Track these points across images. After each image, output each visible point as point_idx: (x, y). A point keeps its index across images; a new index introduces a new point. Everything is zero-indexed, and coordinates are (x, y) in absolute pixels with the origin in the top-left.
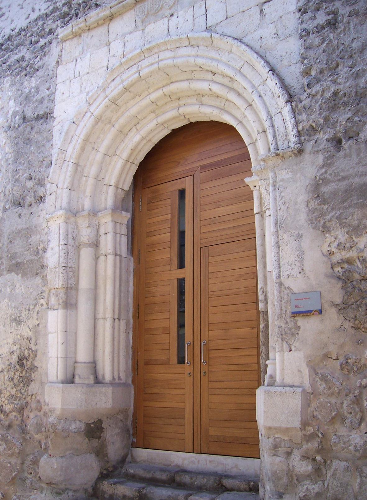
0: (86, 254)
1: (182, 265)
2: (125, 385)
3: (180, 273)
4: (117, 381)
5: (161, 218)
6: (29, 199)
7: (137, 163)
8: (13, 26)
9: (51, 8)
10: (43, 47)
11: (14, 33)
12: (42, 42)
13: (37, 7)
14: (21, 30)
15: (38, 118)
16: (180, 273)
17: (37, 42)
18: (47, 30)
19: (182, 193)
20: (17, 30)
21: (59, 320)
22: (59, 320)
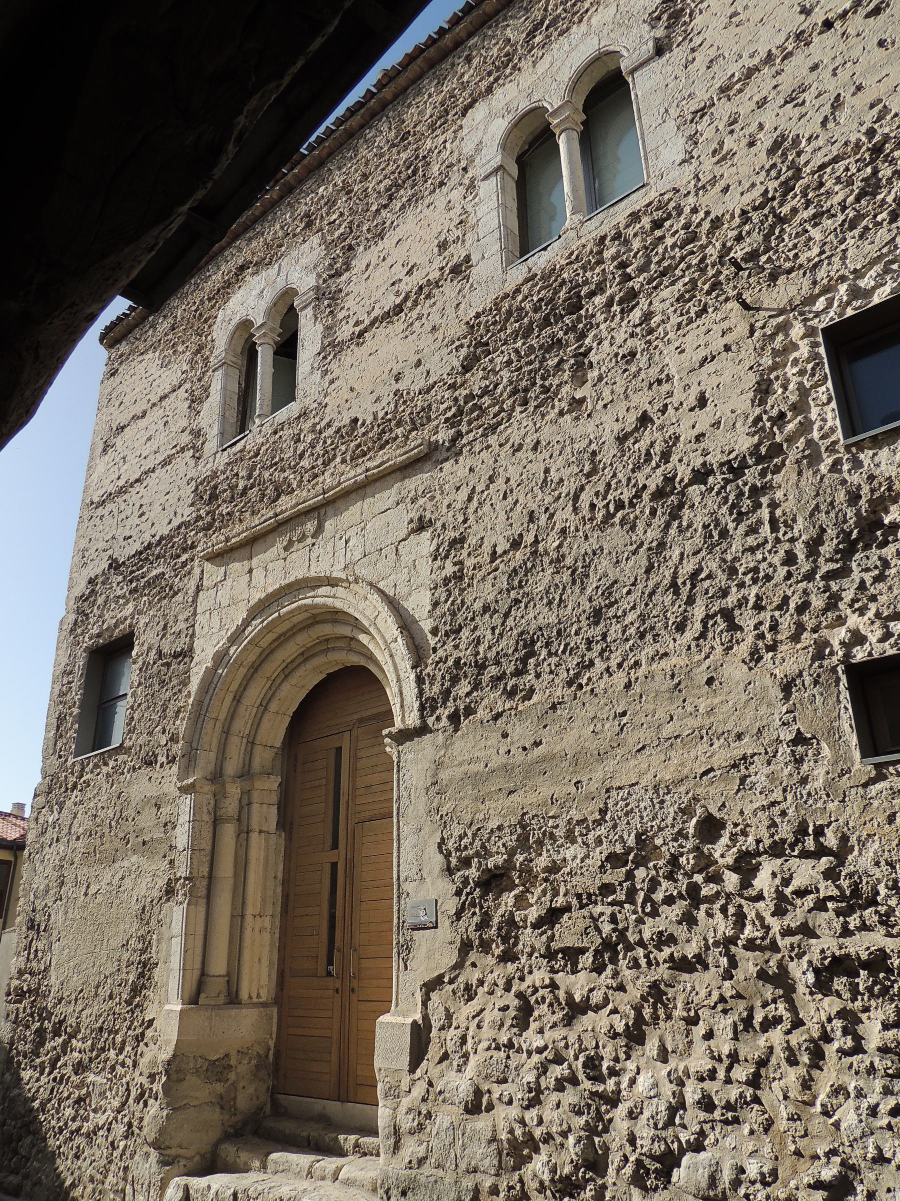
0: (229, 831)
1: (335, 846)
2: (264, 1005)
3: (332, 856)
4: (255, 1000)
5: (317, 783)
6: (162, 759)
7: (291, 713)
8: (153, 532)
9: (194, 515)
10: (184, 564)
11: (153, 541)
12: (184, 558)
13: (179, 511)
14: (162, 538)
15: (176, 656)
16: (332, 856)
17: (178, 556)
18: (189, 543)
19: (339, 750)
20: (157, 538)
21: (311, 502)
22: (311, 502)
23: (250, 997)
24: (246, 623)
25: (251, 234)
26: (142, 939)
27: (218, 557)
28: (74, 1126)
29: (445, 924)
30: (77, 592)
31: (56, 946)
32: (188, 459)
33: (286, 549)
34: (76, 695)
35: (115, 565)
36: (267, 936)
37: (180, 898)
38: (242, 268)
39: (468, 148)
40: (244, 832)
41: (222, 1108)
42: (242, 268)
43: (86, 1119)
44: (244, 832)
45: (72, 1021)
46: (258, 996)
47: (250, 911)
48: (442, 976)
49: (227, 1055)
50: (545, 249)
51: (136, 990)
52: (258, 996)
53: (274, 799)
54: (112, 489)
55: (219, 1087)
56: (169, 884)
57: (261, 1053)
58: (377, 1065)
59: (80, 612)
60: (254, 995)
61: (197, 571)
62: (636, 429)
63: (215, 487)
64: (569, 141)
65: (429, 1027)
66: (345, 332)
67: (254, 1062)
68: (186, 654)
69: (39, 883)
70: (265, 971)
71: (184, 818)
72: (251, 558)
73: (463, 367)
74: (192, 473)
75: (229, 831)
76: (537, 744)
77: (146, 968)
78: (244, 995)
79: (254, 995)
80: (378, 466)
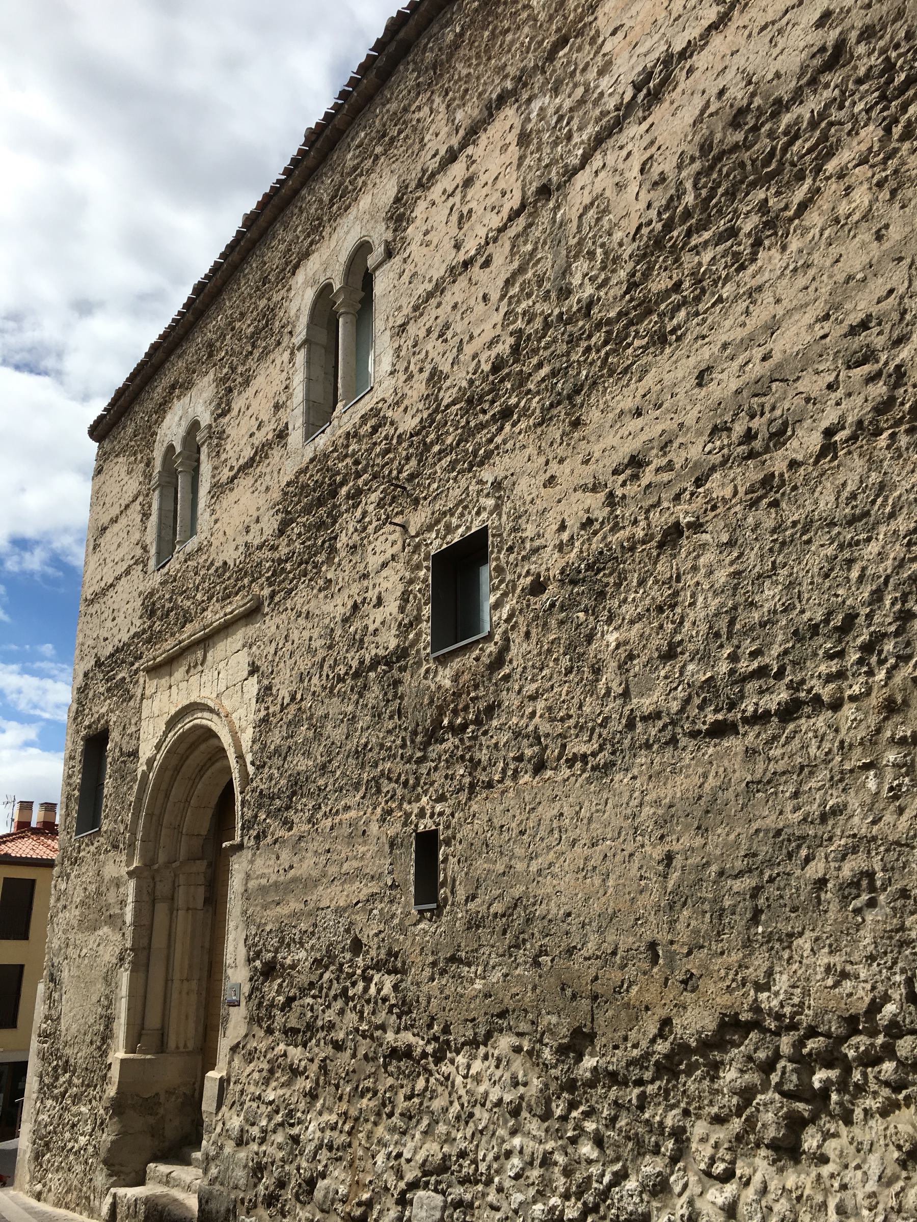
2: (188, 1053)
4: (182, 1049)
23: (177, 1048)
24: (165, 734)
25: (179, 351)
26: (107, 997)
27: (155, 670)
28: (70, 1145)
29: (243, 1003)
30: (77, 685)
31: (64, 997)
32: (139, 572)
33: (188, 672)
34: (77, 780)
35: (99, 664)
36: (194, 997)
37: (127, 966)
38: (173, 387)
39: (293, 312)
40: (172, 911)
41: (153, 1136)
42: (173, 387)
43: (76, 1141)
44: (172, 911)
45: (72, 1061)
46: (185, 1046)
47: (177, 976)
48: (239, 1043)
49: (157, 1094)
50: (323, 432)
51: (104, 1040)
52: (185, 1046)
53: (201, 879)
54: (98, 590)
55: (151, 1120)
56: (121, 953)
57: (188, 1092)
58: (204, 1108)
59: (80, 703)
60: (181, 1045)
61: (141, 681)
62: (351, 615)
63: (154, 604)
64: (345, 323)
65: (228, 1080)
66: (226, 474)
67: (180, 1100)
68: (134, 754)
69: (56, 944)
70: (191, 1025)
71: (130, 899)
72: (171, 676)
73: (279, 530)
74: (141, 588)
75: (162, 909)
76: (291, 867)
77: (109, 1020)
78: (172, 1044)
79: (181, 1045)
80: (231, 613)
